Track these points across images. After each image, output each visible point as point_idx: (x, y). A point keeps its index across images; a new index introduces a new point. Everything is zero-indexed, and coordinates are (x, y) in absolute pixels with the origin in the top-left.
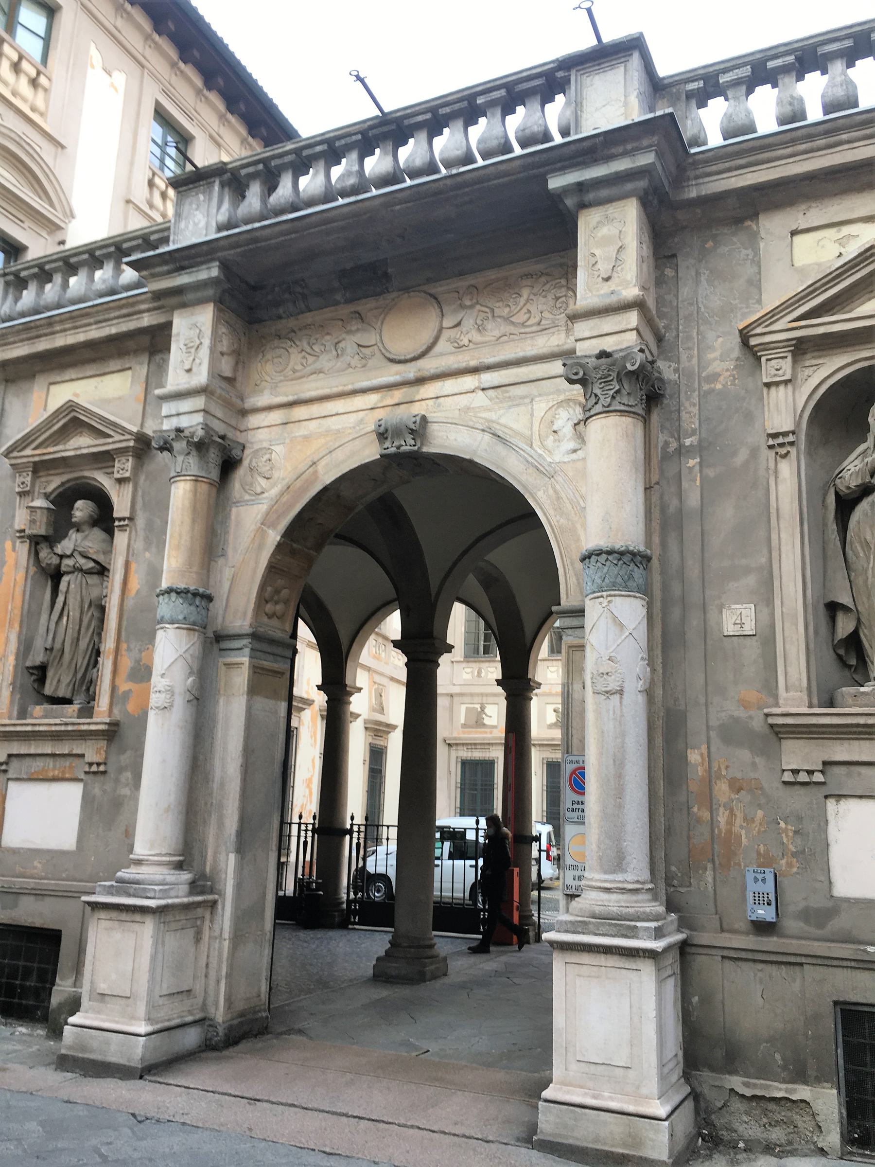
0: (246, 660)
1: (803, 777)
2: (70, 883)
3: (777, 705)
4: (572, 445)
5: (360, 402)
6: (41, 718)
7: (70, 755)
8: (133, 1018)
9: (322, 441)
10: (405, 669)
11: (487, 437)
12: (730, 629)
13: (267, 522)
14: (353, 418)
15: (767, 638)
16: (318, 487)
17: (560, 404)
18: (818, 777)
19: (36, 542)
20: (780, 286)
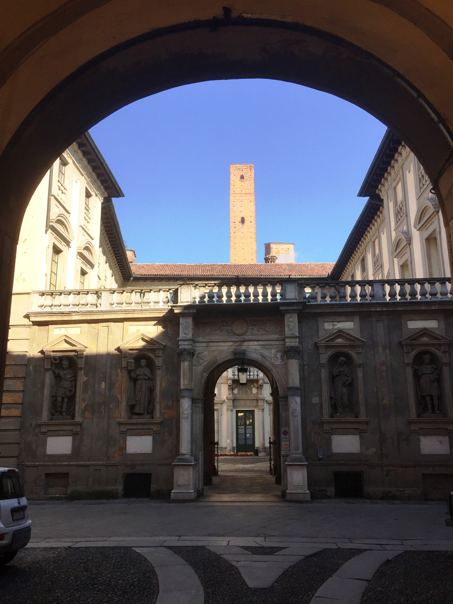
0: (200, 405)
1: (327, 431)
2: (180, 463)
3: (323, 417)
4: (281, 361)
5: (227, 344)
6: (135, 419)
7: (148, 429)
8: (189, 489)
9: (218, 352)
10: (112, 349)
11: (261, 356)
12: (314, 402)
13: (204, 371)
14: (226, 347)
15: (321, 405)
16: (217, 364)
17: (277, 351)
18: (330, 431)
19: (129, 372)
20: (322, 335)
